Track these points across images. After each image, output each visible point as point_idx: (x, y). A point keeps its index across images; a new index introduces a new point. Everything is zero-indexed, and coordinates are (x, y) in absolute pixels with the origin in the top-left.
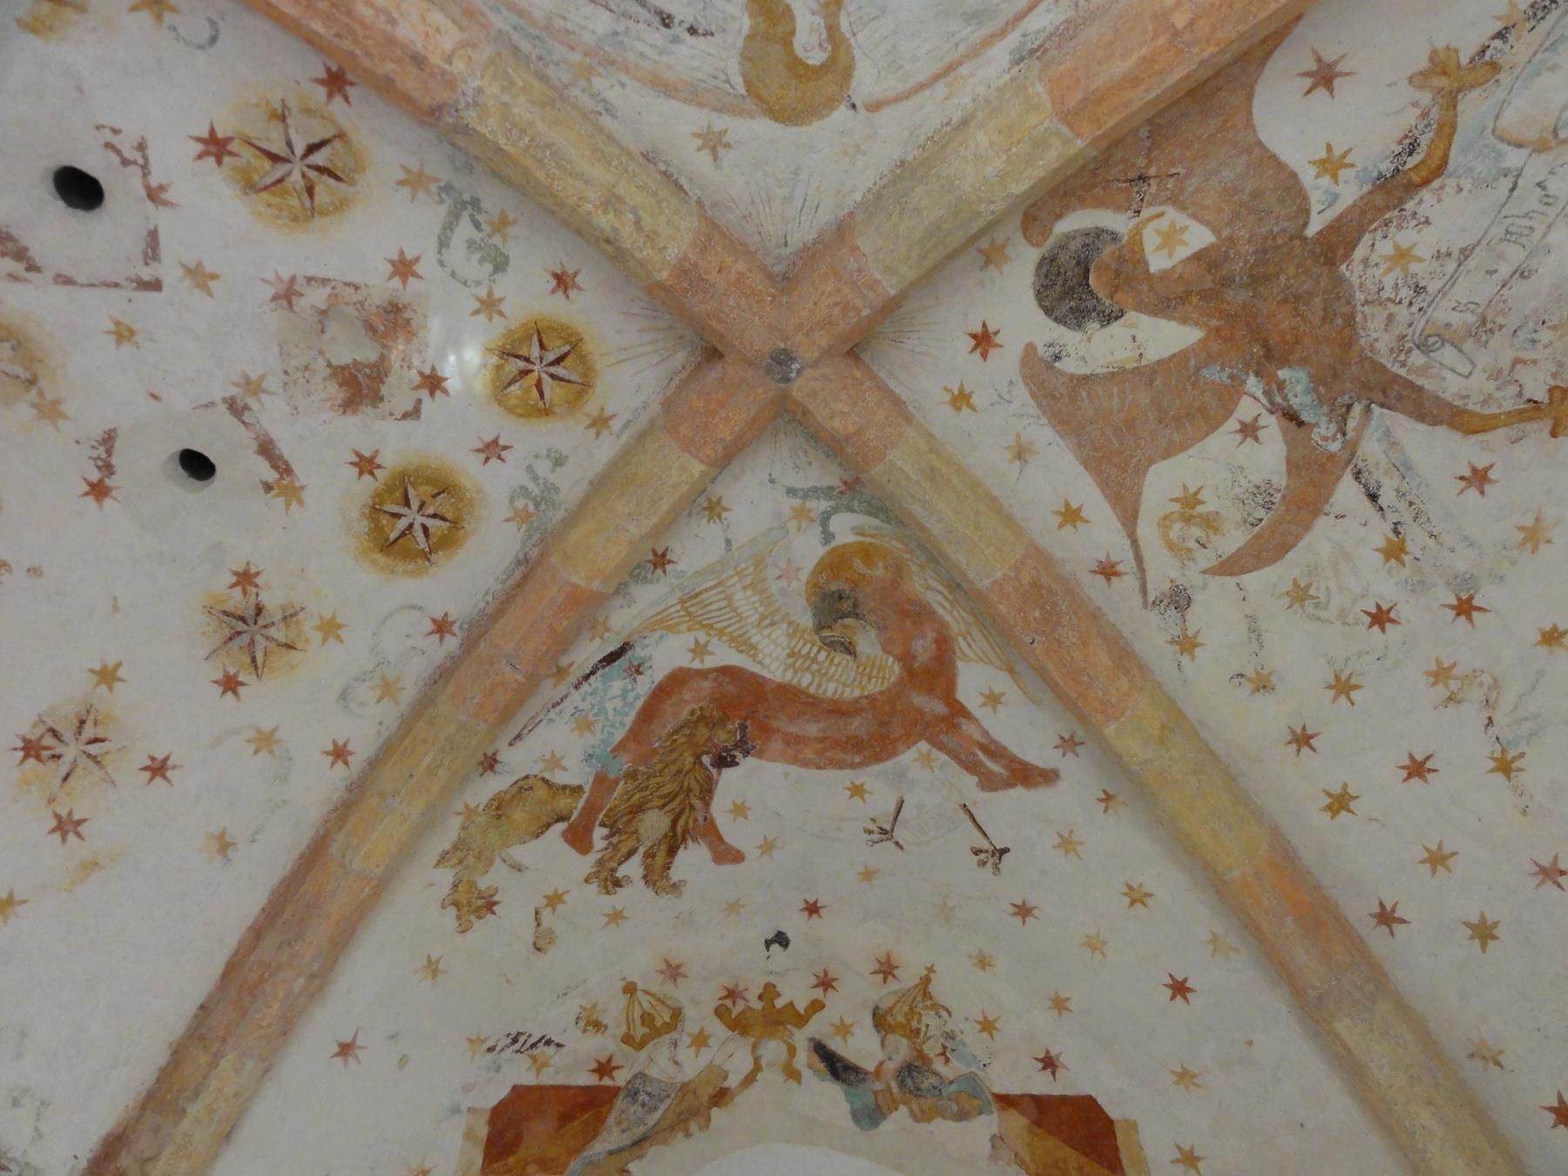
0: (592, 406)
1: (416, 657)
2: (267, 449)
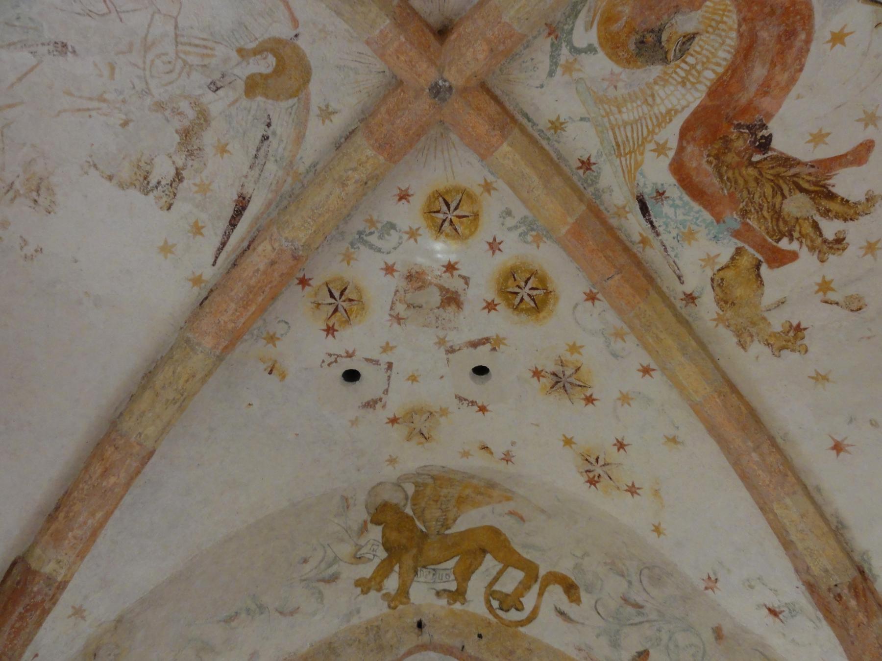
0: (477, 190)
1: (601, 317)
2: (474, 345)
